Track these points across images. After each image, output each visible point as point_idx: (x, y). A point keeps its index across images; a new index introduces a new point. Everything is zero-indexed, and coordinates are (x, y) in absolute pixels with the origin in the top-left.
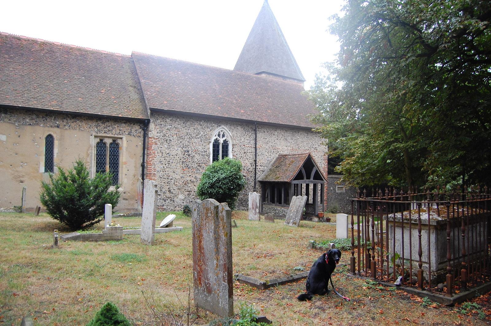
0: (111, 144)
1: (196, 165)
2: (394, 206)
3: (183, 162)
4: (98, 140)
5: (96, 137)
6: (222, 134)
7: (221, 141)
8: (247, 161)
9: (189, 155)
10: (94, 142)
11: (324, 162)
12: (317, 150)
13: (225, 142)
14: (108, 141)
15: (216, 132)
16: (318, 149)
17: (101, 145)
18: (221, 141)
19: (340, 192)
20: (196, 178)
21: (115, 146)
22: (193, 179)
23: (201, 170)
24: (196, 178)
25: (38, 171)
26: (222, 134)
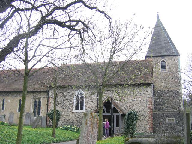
0: (38, 101)
1: (67, 108)
2: (30, 31)
3: (62, 107)
4: (34, 100)
5: (33, 99)
6: (80, 93)
7: (80, 96)
8: (93, 105)
9: (64, 104)
10: (32, 101)
11: (149, 103)
12: (142, 96)
13: (82, 97)
14: (37, 100)
15: (77, 92)
16: (144, 96)
17: (35, 102)
18: (80, 96)
19: (170, 122)
20: (67, 114)
21: (40, 102)
22: (66, 114)
23: (70, 110)
24: (67, 114)
25: (16, 111)
26: (80, 93)
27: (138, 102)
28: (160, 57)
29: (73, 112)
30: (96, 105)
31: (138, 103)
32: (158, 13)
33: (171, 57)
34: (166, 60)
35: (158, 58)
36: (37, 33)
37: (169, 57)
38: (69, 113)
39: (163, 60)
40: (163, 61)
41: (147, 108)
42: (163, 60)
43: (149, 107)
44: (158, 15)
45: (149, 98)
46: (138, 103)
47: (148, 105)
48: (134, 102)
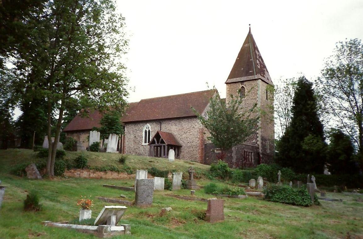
11: (199, 134)
16: (195, 127)
24: (138, 147)
27: (191, 133)
28: (240, 83)
29: (142, 145)
30: (36, 168)
31: (191, 135)
32: (250, 25)
33: (251, 82)
34: (245, 85)
35: (237, 84)
36: (296, 101)
37: (249, 82)
38: (139, 146)
39: (242, 85)
40: (243, 87)
41: (197, 139)
42: (242, 85)
43: (199, 138)
44: (250, 27)
45: (200, 129)
46: (191, 135)
47: (199, 136)
48: (188, 133)
